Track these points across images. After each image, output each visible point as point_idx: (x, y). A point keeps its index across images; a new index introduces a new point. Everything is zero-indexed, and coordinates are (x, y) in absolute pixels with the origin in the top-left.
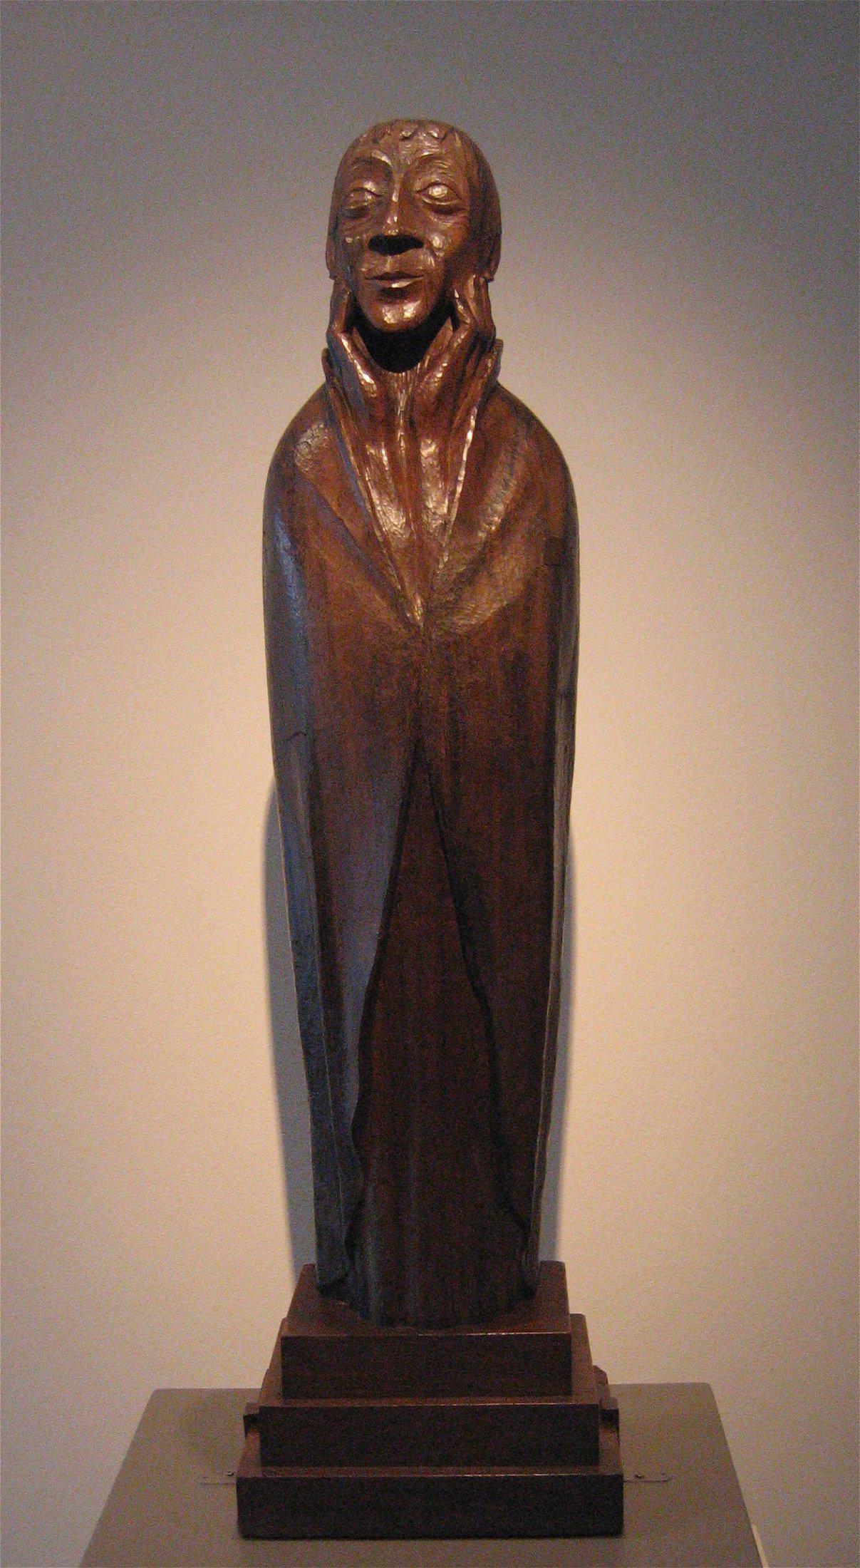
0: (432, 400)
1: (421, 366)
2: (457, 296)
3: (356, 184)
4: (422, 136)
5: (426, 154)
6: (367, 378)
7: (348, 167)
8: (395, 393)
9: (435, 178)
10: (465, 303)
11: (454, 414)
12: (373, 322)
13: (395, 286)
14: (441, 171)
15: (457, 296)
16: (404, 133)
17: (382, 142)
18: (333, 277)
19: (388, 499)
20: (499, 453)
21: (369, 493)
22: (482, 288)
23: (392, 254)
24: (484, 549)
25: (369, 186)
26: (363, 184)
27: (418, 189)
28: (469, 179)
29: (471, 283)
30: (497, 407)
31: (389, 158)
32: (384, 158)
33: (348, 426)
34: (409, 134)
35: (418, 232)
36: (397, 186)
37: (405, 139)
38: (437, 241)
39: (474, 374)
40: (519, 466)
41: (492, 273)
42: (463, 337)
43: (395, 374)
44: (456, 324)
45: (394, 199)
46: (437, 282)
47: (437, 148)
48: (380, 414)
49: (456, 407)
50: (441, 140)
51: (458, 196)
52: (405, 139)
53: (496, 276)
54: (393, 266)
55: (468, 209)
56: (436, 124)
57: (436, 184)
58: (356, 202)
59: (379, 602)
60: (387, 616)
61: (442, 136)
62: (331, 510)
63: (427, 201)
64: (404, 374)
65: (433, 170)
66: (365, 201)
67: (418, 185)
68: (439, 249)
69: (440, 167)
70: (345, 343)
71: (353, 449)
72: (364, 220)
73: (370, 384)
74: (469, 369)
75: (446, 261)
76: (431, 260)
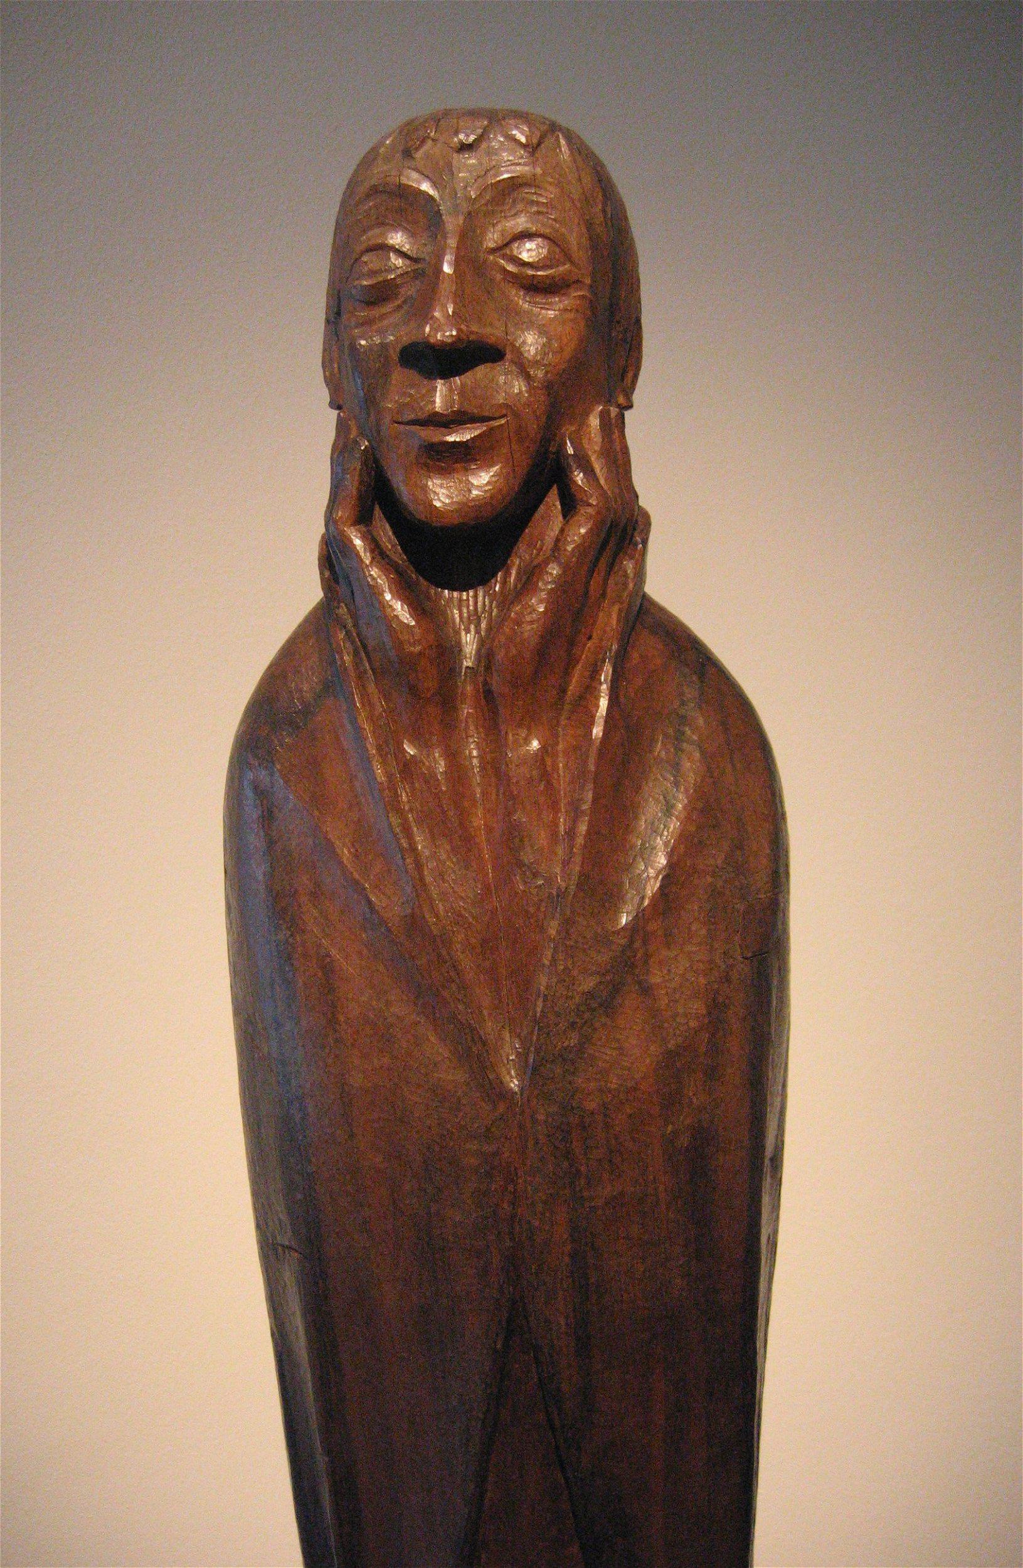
0: (527, 655)
1: (504, 583)
2: (570, 451)
3: (373, 236)
4: (497, 140)
5: (506, 176)
6: (400, 610)
7: (357, 205)
8: (458, 633)
9: (521, 222)
10: (589, 472)
11: (567, 673)
12: (412, 507)
13: (450, 439)
14: (535, 209)
15: (570, 451)
16: (462, 136)
17: (419, 155)
18: (336, 405)
19: (448, 847)
20: (653, 741)
21: (410, 836)
22: (614, 428)
23: (444, 376)
24: (632, 942)
25: (397, 239)
26: (383, 235)
27: (492, 245)
28: (589, 225)
29: (594, 421)
30: (648, 645)
31: (435, 185)
32: (426, 187)
33: (365, 695)
34: (472, 138)
35: (492, 331)
36: (452, 242)
37: (464, 148)
38: (531, 343)
39: (604, 595)
40: (691, 766)
41: (629, 392)
42: (583, 531)
43: (455, 594)
44: (570, 505)
45: (447, 269)
46: (533, 427)
47: (525, 164)
48: (429, 684)
49: (570, 663)
50: (532, 148)
51: (568, 258)
52: (464, 148)
53: (636, 397)
54: (448, 401)
55: (588, 281)
56: (522, 116)
57: (526, 235)
58: (373, 273)
59: (435, 1048)
60: (453, 1076)
61: (535, 141)
62: (341, 863)
63: (510, 268)
64: (471, 593)
65: (520, 206)
66: (390, 270)
67: (492, 239)
68: (536, 363)
69: (532, 202)
70: (358, 542)
71: (379, 748)
72: (387, 308)
73: (407, 626)
74: (594, 585)
75: (548, 386)
76: (518, 386)
